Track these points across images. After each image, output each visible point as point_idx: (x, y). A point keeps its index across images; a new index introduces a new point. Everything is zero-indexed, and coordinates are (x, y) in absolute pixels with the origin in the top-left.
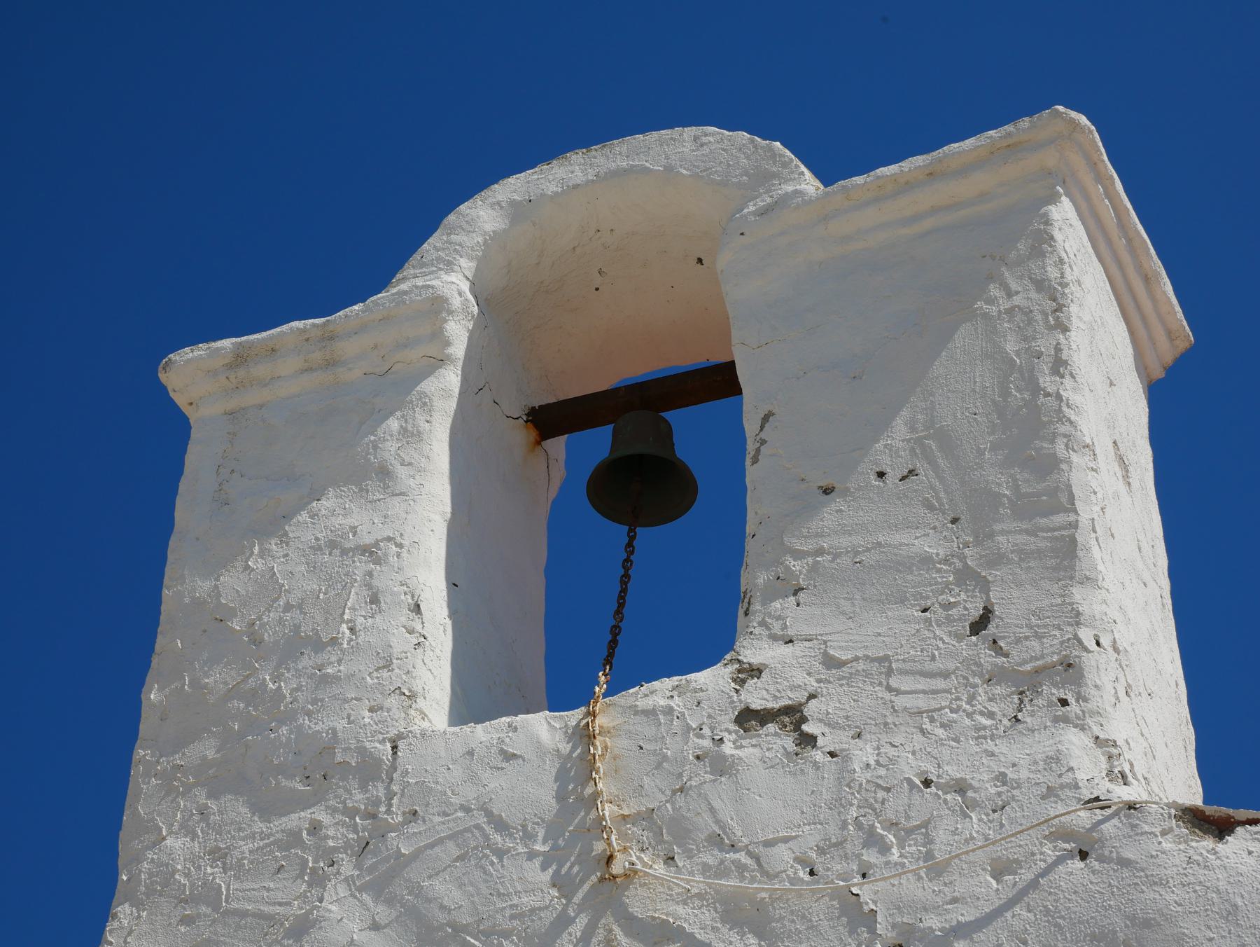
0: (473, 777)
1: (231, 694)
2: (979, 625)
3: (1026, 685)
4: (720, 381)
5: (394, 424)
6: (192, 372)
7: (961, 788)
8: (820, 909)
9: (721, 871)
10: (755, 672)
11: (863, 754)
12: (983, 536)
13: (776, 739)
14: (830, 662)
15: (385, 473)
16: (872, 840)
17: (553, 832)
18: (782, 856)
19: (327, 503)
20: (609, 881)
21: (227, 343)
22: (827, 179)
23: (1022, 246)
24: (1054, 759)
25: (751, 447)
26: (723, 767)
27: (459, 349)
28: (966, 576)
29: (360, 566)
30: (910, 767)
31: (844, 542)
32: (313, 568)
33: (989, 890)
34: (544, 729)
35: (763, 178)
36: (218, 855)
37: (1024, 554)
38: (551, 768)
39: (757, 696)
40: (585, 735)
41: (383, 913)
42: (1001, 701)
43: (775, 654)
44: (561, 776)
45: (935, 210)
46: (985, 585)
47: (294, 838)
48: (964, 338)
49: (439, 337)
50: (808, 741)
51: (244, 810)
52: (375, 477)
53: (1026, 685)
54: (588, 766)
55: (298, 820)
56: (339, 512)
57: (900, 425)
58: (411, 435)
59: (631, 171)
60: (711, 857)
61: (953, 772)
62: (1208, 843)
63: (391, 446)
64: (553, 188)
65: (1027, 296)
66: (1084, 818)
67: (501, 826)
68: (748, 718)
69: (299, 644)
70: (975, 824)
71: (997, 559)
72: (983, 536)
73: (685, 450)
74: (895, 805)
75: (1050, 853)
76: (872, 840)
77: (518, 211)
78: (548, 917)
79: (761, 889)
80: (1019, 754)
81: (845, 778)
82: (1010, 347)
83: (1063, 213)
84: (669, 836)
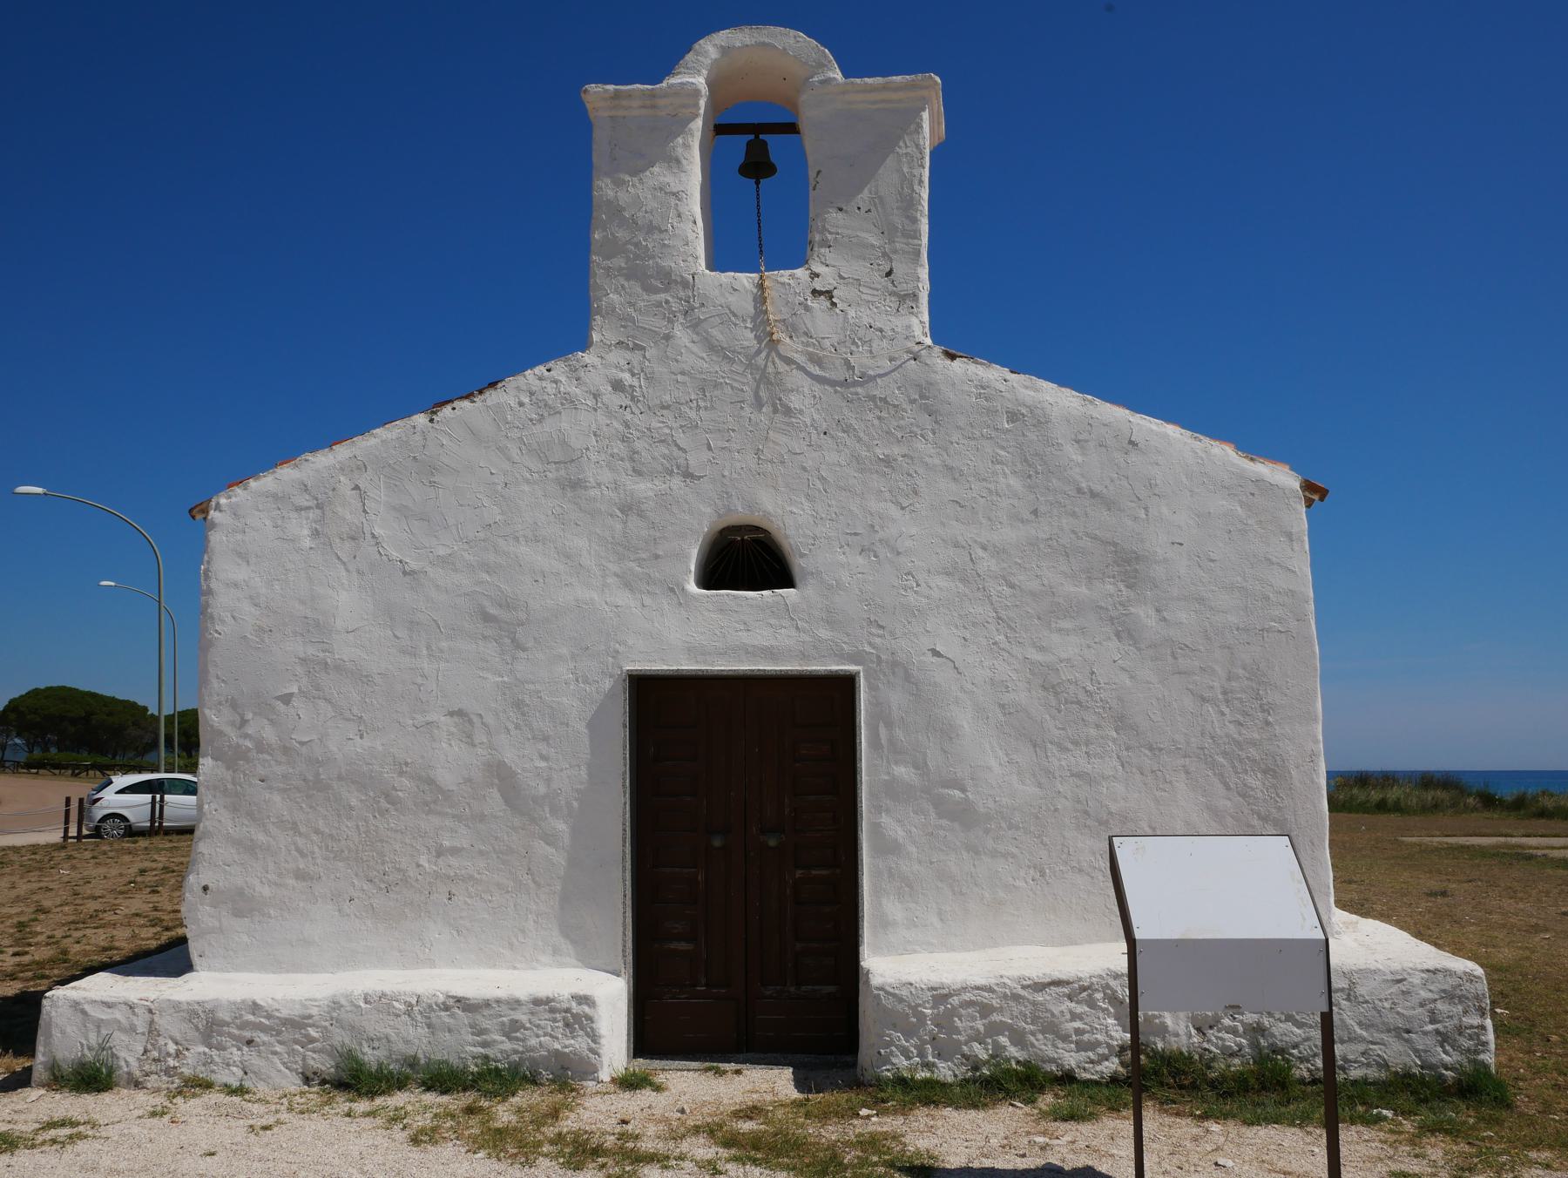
0: (723, 295)
1: (627, 242)
2: (889, 274)
3: (902, 298)
4: (791, 128)
5: (680, 140)
6: (597, 93)
7: (881, 330)
8: (838, 362)
9: (808, 345)
10: (818, 275)
11: (852, 313)
12: (891, 242)
13: (823, 302)
14: (841, 277)
15: (678, 161)
16: (854, 343)
17: (754, 320)
18: (827, 343)
19: (656, 169)
20: (773, 344)
21: (611, 87)
22: (846, 75)
23: (913, 127)
24: (909, 327)
25: (812, 182)
26: (807, 309)
27: (702, 111)
28: (885, 254)
29: (673, 201)
30: (866, 321)
31: (846, 232)
32: (655, 197)
33: (888, 365)
34: (746, 280)
35: (821, 66)
36: (631, 304)
37: (904, 252)
38: (750, 298)
39: (818, 285)
40: (761, 287)
41: (695, 338)
42: (892, 302)
43: (826, 268)
44: (755, 300)
45: (883, 101)
46: (891, 260)
47: (659, 305)
48: (890, 161)
49: (697, 106)
50: (834, 304)
51: (639, 290)
52: (675, 163)
53: (902, 298)
54: (764, 300)
55: (662, 296)
56: (659, 174)
57: (866, 191)
58: (687, 146)
59: (768, 45)
60: (804, 339)
61: (879, 325)
62: (948, 362)
63: (680, 150)
64: (738, 44)
65: (912, 150)
66: (917, 348)
67: (735, 315)
68: (816, 293)
69: (651, 229)
70: (885, 343)
71: (895, 252)
72: (891, 242)
73: (774, 157)
74: (861, 333)
75: (906, 357)
76: (854, 343)
77: (725, 51)
78: (753, 350)
79: (821, 354)
80: (899, 323)
81: (846, 319)
82: (905, 170)
83: (925, 115)
84: (792, 331)
